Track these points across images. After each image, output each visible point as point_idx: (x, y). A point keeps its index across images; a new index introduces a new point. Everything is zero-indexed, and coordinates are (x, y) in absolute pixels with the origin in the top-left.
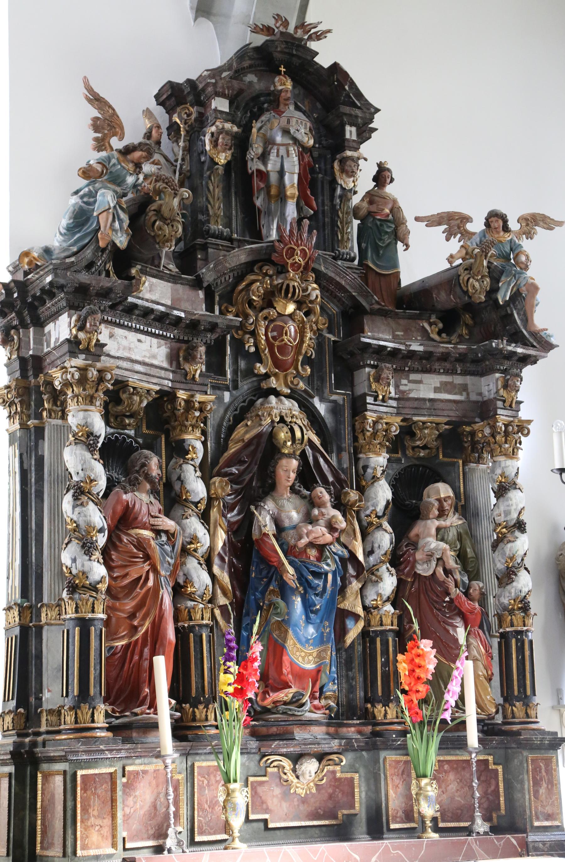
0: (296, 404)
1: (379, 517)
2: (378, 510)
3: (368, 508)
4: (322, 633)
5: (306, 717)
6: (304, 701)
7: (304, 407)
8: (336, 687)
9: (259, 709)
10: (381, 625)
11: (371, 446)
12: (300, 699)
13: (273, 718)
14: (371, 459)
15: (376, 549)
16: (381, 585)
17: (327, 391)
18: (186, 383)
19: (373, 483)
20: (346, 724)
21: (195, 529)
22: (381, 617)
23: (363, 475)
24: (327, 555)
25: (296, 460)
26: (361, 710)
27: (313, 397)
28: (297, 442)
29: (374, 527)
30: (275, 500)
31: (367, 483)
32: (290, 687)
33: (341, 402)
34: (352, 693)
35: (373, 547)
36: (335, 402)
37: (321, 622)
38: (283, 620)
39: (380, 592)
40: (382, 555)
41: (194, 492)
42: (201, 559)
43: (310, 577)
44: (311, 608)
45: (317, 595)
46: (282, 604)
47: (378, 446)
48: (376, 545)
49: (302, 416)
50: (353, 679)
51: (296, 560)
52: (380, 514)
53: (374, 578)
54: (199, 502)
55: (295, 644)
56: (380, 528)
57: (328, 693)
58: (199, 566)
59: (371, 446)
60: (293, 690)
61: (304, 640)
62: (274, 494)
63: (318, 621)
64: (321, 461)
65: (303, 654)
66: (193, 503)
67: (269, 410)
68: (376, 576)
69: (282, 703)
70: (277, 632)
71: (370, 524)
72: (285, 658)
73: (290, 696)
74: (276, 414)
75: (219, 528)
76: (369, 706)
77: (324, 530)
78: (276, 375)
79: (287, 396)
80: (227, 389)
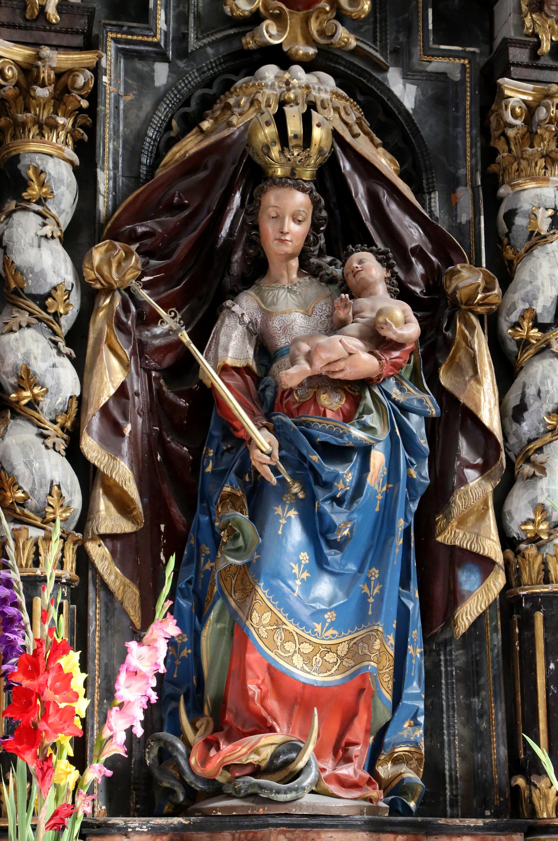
0: (330, 81)
1: (544, 328)
2: (539, 309)
3: (514, 307)
4: (365, 597)
5: (301, 807)
6: (301, 765)
7: (363, 93)
8: (420, 732)
9: (199, 786)
10: (547, 581)
11: (524, 163)
12: (293, 760)
13: (222, 809)
14: (525, 195)
15: (530, 400)
16: (543, 484)
17: (417, 51)
18: (25, 28)
19: (529, 250)
20: (447, 826)
21: (27, 355)
22: (545, 563)
23: (507, 235)
24: (366, 406)
25: (303, 190)
26: (502, 793)
27: (384, 69)
28: (292, 143)
29: (532, 351)
30: (260, 294)
31: (516, 253)
32: (272, 730)
33: (457, 76)
34: (479, 749)
35: (523, 395)
36: (442, 76)
37: (361, 570)
38: (249, 564)
39: (541, 500)
40: (549, 414)
41: (32, 270)
42: (48, 425)
43: (315, 458)
44: (331, 537)
45: (339, 502)
46: (249, 528)
47: (541, 162)
48: (531, 391)
49: (340, 103)
50: (481, 716)
51: (289, 420)
52: (548, 319)
53: (528, 469)
54: (49, 295)
55: (278, 624)
56: (547, 353)
57: (401, 749)
58: (40, 440)
59: (524, 163)
60: (276, 738)
61: (304, 613)
62: (264, 282)
63: (352, 567)
64: (385, 197)
65: (307, 648)
66: (34, 298)
67: (254, 90)
68: (534, 464)
69: (248, 770)
70: (238, 595)
71: (524, 344)
72: (251, 657)
73: (267, 753)
74: (268, 100)
75: (106, 353)
76: (521, 781)
77: (355, 344)
78: (279, 19)
79: (309, 67)
80: (162, 57)
